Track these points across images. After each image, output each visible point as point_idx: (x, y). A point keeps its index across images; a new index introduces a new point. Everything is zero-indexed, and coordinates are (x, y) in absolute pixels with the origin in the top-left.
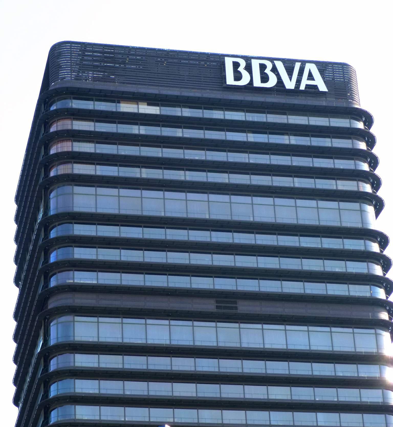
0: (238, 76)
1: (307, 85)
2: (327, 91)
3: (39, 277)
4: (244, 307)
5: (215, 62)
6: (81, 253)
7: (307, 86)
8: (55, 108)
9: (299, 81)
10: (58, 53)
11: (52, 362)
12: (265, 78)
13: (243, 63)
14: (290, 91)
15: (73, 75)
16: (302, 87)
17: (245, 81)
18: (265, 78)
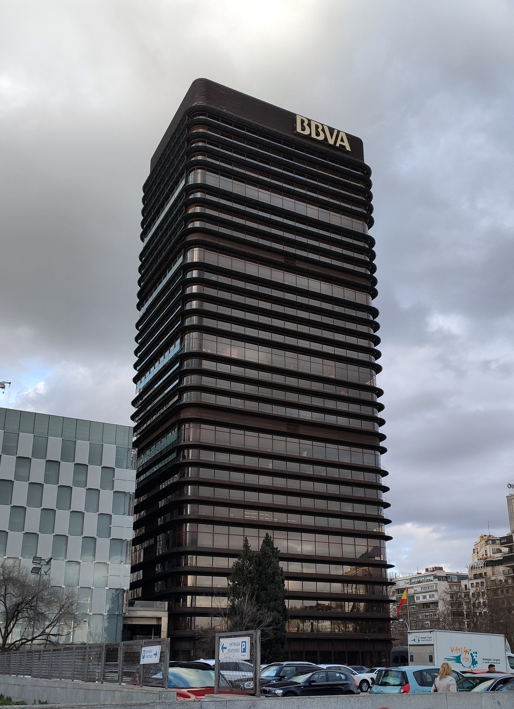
0: (303, 129)
5: (291, 117)
6: (208, 381)
9: (336, 142)
12: (318, 134)
13: (306, 122)
14: (330, 145)
16: (338, 145)
18: (318, 134)
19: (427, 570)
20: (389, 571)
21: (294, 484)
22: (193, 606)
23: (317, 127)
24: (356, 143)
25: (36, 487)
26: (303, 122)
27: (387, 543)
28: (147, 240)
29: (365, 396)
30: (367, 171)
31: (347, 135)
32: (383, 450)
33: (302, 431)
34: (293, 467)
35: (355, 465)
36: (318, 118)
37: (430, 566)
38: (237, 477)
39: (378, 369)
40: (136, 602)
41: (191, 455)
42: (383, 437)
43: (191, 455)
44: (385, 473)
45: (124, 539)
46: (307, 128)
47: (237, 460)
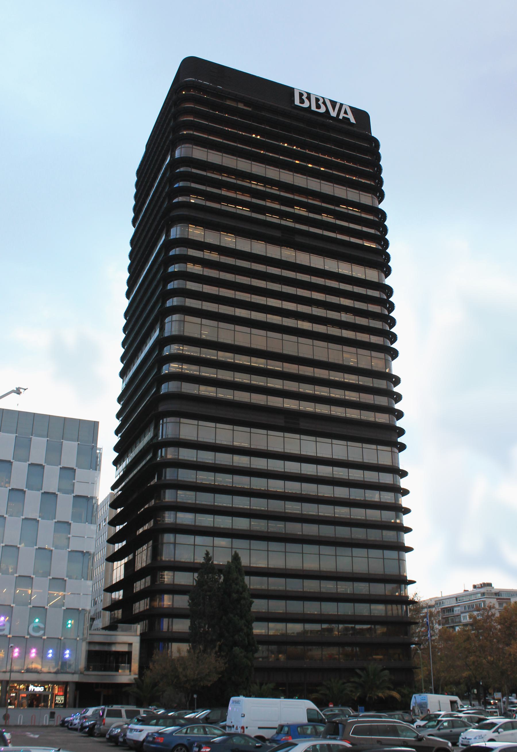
0: (302, 101)
2: (355, 122)
3: (164, 199)
4: (299, 239)
5: (290, 91)
6: (191, 268)
7: (343, 117)
8: (174, 253)
11: (163, 386)
12: (318, 107)
13: (305, 95)
15: (175, 590)
16: (341, 117)
18: (318, 107)
19: (475, 587)
20: (410, 587)
21: (357, 494)
22: (170, 630)
23: (317, 100)
24: (362, 117)
25: (49, 497)
26: (301, 95)
27: (408, 556)
28: (127, 379)
29: (382, 384)
30: (376, 143)
31: (351, 108)
32: (402, 447)
33: (304, 424)
36: (316, 91)
37: (478, 582)
38: (325, 491)
39: (394, 354)
40: (119, 625)
41: (170, 453)
42: (401, 432)
43: (170, 453)
44: (404, 474)
45: (85, 551)
46: (306, 101)
47: (207, 457)
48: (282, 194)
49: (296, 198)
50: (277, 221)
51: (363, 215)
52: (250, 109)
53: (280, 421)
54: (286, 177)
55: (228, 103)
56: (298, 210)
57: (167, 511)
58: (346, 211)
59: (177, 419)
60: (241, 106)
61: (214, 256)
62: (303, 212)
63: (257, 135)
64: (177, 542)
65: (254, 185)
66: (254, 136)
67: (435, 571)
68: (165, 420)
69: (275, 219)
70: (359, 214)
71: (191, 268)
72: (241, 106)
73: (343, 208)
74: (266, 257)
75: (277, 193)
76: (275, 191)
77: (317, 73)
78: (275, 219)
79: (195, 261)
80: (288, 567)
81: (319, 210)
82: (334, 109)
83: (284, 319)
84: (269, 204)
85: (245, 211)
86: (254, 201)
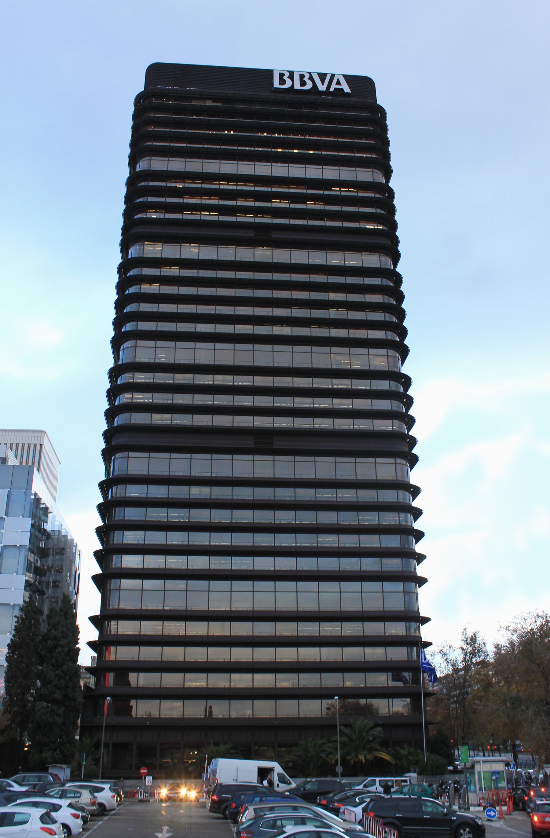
0: (282, 82)
1: (335, 88)
4: (276, 235)
6: (146, 288)
10: (157, 73)
12: (303, 83)
14: (322, 93)
16: (332, 89)
17: (288, 84)
18: (303, 83)
21: (347, 518)
31: (344, 76)
33: (278, 444)
34: (264, 629)
35: (199, 501)
36: (300, 66)
48: (257, 189)
49: (274, 190)
50: (251, 220)
51: (360, 194)
52: (220, 104)
53: (249, 443)
54: (263, 169)
55: (195, 103)
56: (276, 203)
57: (115, 554)
58: (339, 193)
59: (126, 454)
60: (209, 103)
61: (174, 271)
62: (284, 205)
63: (229, 131)
64: (121, 588)
65: (224, 186)
66: (226, 132)
67: (468, 603)
68: (117, 456)
69: (249, 219)
70: (356, 194)
71: (146, 288)
72: (209, 103)
73: (335, 191)
74: (291, 264)
75: (252, 188)
76: (249, 188)
77: (296, 48)
78: (249, 219)
79: (151, 280)
80: (277, 609)
81: (303, 198)
82: (323, 83)
83: (256, 327)
84: (241, 203)
85: (213, 217)
86: (222, 202)
